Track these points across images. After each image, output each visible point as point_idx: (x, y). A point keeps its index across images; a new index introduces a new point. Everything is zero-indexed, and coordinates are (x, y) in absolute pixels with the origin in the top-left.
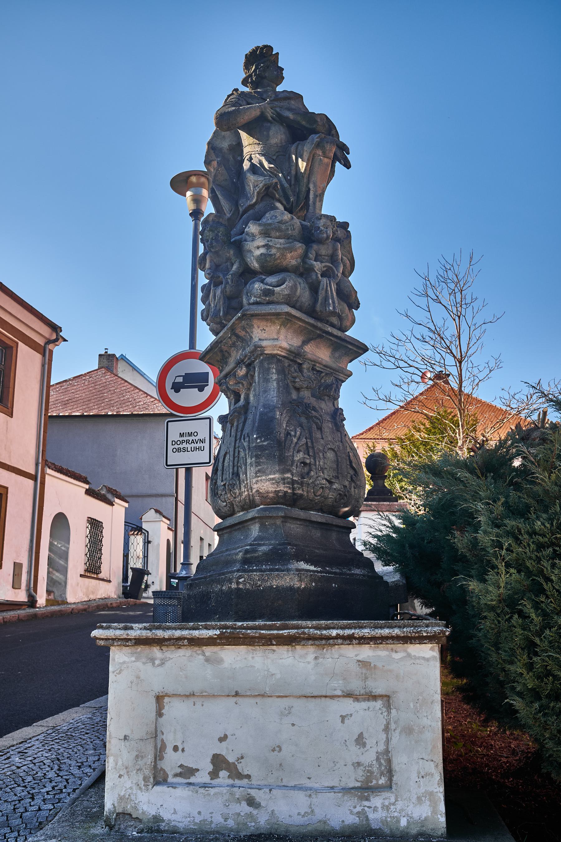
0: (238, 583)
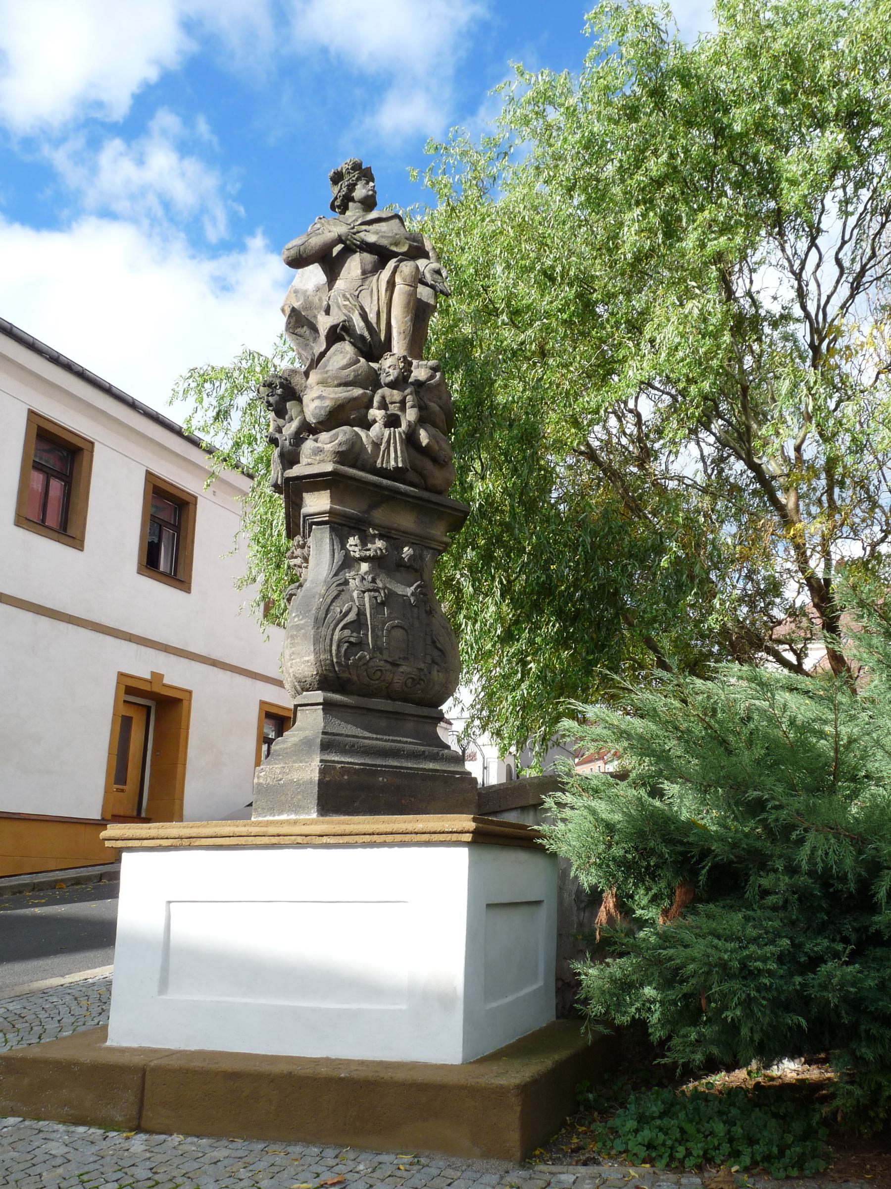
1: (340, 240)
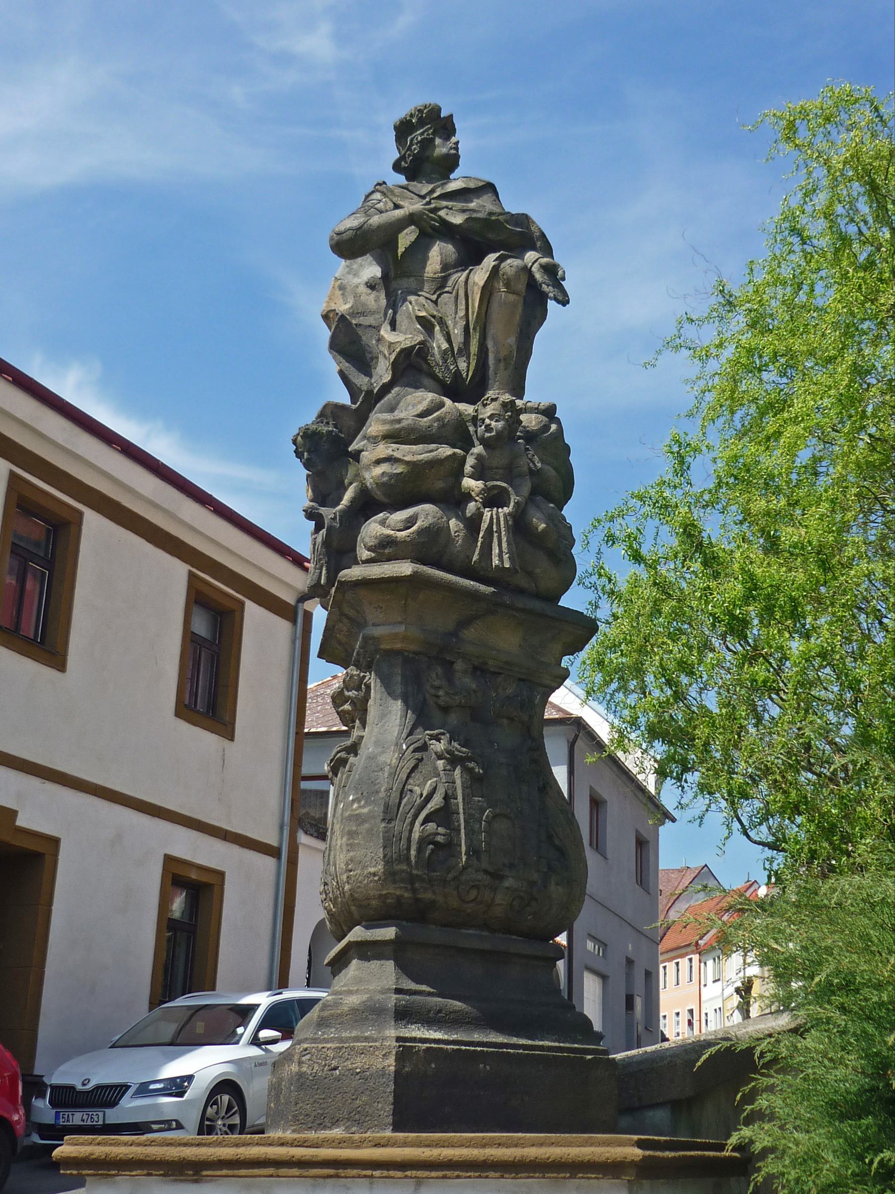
0: (300, 1063)
1: (412, 219)
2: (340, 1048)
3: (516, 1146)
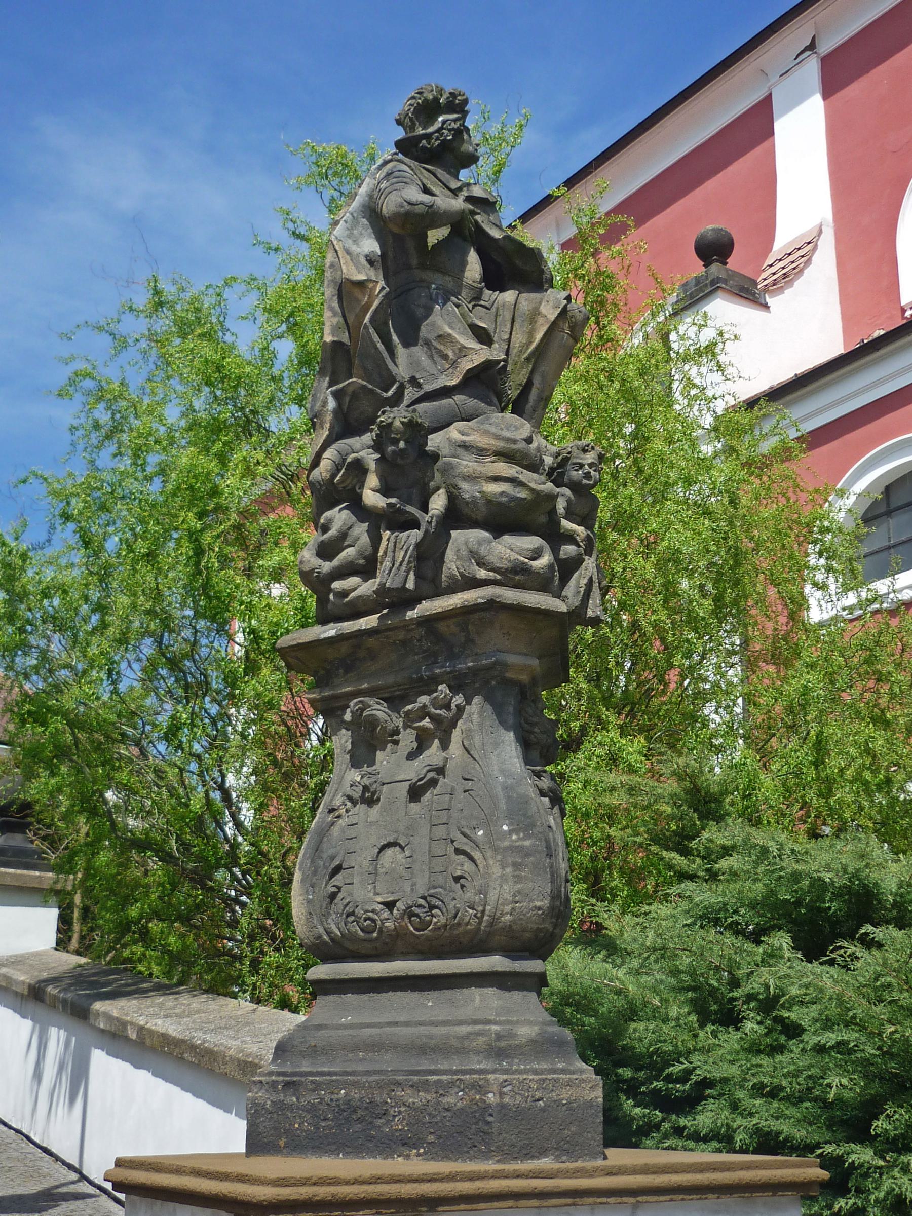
2: (544, 1080)
3: (728, 1170)
